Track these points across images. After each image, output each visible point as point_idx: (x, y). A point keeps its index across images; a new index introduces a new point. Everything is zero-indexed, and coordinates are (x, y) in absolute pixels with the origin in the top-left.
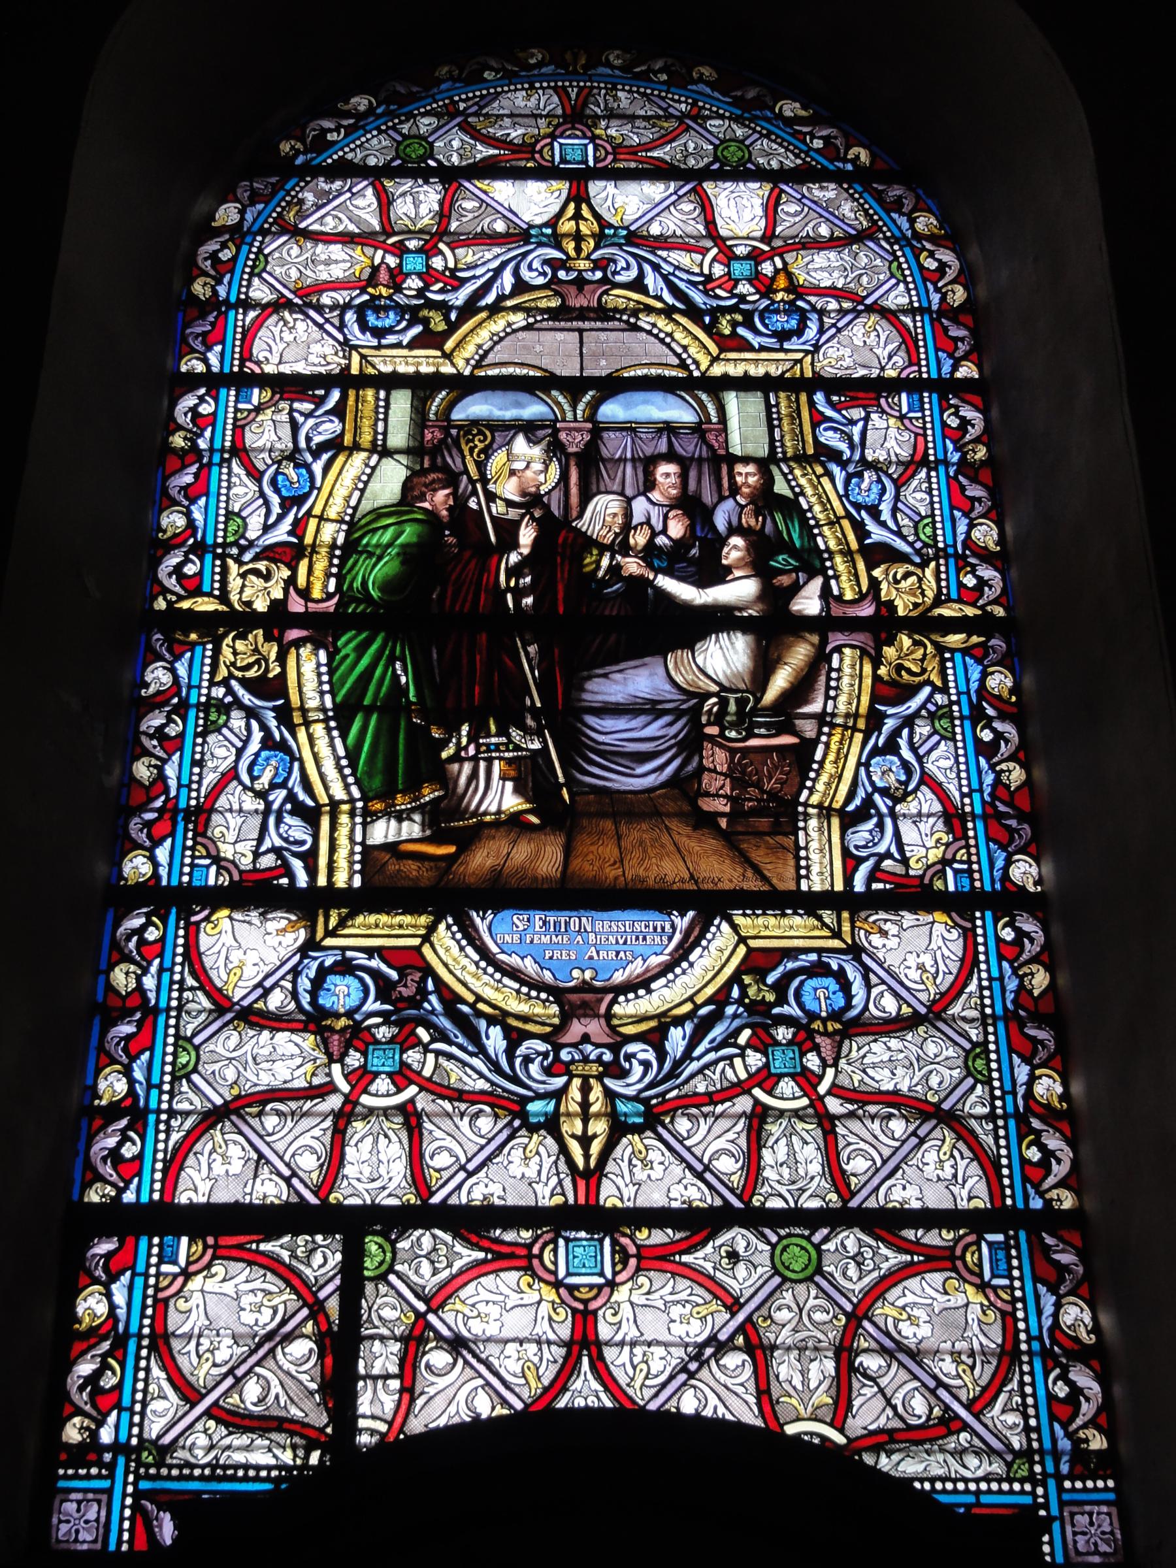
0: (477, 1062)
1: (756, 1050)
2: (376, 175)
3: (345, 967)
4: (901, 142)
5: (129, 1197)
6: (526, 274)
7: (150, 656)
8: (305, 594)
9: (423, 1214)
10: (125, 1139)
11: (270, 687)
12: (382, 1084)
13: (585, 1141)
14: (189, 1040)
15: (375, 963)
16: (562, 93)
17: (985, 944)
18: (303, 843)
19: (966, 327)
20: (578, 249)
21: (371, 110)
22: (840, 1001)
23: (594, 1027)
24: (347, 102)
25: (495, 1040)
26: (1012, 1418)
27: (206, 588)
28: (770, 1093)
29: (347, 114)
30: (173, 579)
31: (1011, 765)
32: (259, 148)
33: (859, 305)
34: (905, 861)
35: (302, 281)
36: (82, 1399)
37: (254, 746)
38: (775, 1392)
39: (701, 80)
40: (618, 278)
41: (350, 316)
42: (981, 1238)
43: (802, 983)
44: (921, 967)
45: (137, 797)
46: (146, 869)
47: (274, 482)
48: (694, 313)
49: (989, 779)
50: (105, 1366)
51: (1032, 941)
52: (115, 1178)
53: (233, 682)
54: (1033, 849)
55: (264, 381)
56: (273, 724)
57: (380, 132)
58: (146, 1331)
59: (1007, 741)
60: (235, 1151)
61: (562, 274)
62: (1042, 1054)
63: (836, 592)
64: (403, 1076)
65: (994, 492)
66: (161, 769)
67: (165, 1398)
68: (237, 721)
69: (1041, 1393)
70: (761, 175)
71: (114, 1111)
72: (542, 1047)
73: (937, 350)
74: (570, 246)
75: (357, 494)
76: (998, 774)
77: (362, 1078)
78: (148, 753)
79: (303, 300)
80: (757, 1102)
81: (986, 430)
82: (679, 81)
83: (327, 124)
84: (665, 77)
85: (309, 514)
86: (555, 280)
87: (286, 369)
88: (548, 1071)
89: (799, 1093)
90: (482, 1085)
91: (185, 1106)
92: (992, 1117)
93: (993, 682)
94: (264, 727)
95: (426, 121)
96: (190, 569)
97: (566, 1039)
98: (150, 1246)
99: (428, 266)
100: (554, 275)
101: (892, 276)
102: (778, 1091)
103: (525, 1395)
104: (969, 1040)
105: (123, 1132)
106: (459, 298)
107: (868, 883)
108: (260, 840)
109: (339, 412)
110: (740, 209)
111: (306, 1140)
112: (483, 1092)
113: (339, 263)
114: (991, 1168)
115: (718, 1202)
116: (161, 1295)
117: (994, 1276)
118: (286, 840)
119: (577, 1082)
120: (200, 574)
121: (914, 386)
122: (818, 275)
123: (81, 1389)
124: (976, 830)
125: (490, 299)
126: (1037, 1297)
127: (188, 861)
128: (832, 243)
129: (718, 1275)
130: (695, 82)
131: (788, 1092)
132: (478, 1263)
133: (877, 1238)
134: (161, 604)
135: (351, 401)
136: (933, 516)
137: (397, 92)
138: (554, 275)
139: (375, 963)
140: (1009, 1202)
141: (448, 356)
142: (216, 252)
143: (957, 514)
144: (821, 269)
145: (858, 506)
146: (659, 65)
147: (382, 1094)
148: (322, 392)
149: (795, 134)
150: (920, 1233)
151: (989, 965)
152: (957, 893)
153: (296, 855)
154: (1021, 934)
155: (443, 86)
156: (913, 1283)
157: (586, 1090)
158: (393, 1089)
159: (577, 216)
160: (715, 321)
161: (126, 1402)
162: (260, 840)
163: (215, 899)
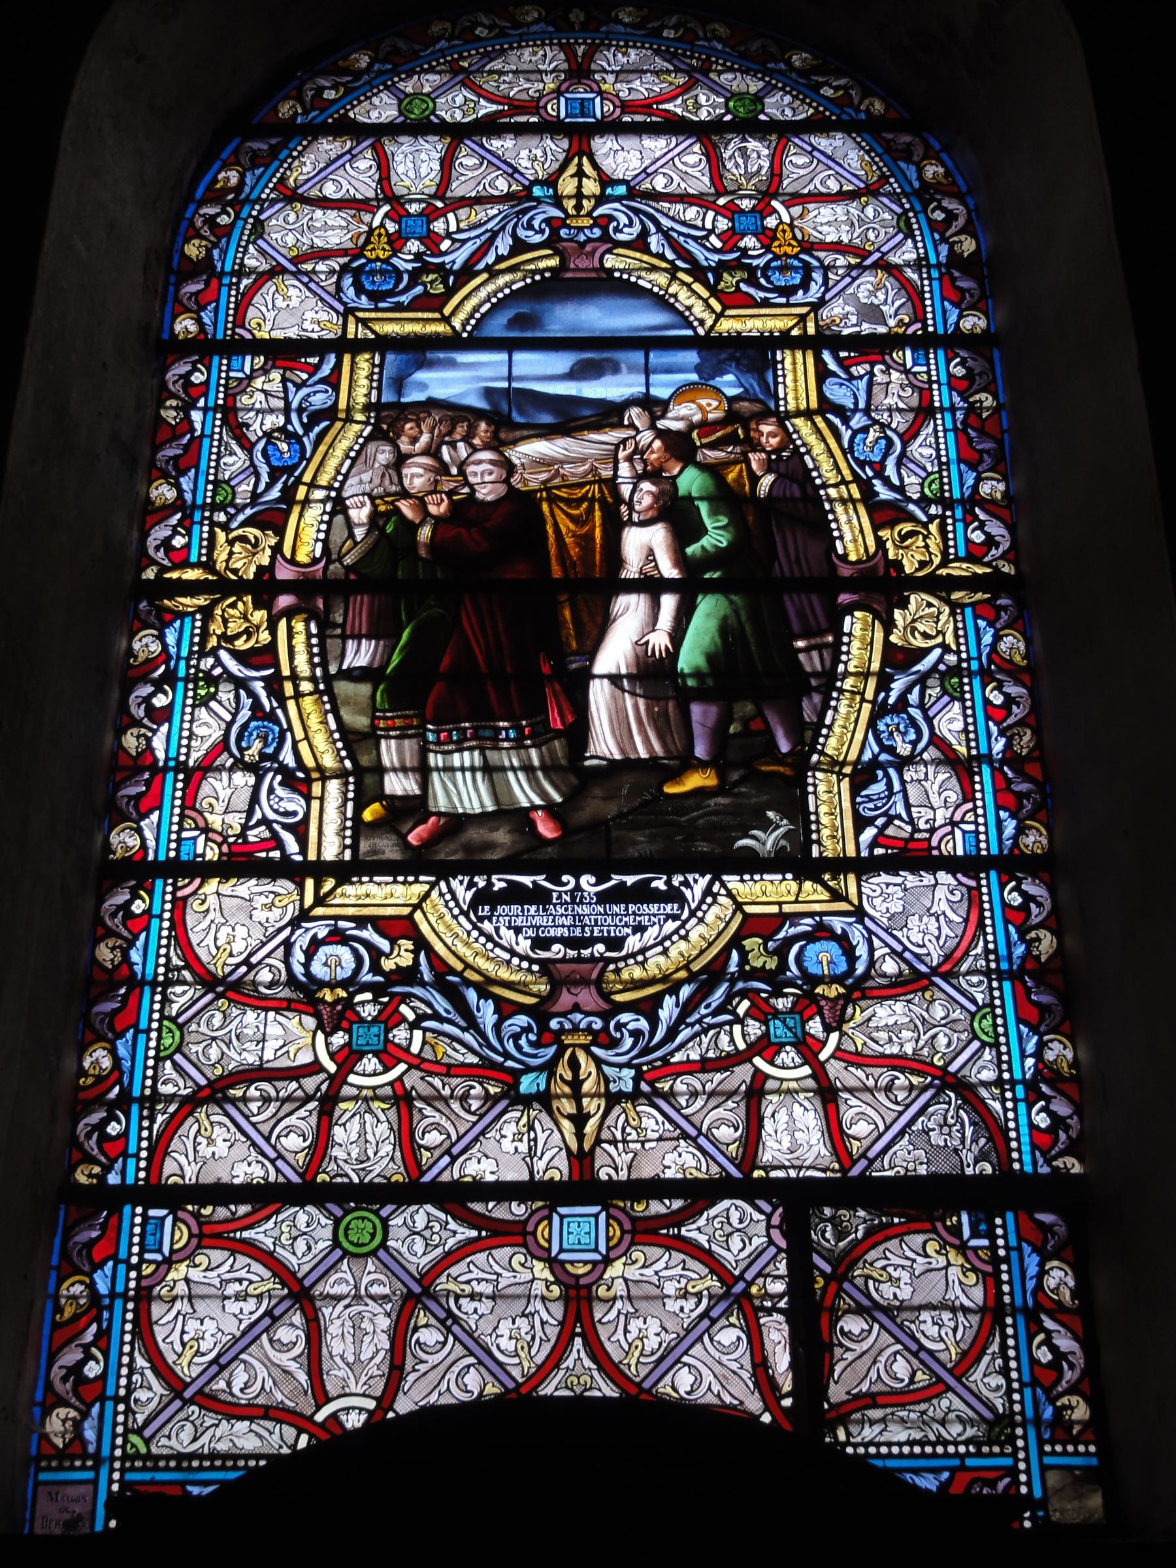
0: (468, 1037)
2: (708, 134)
3: (338, 937)
4: (911, 111)
5: (113, 1179)
7: (178, 308)
8: (292, 561)
9: (411, 1191)
10: (175, 532)
11: (263, 656)
12: (370, 1063)
14: (173, 1020)
15: (369, 934)
17: (991, 910)
18: (295, 813)
19: (1024, 686)
20: (579, 207)
22: (843, 967)
23: (587, 997)
25: (487, 1014)
27: (193, 558)
28: (771, 1063)
29: (345, 71)
30: (161, 554)
32: (254, 117)
33: (864, 260)
35: (296, 248)
36: (177, 388)
37: (245, 714)
40: (620, 237)
41: (348, 281)
43: (802, 949)
45: (163, 434)
46: (193, 328)
47: (264, 453)
48: (698, 271)
51: (1039, 905)
52: (125, 933)
55: (257, 346)
56: (263, 695)
58: (167, 915)
60: (219, 1133)
62: (1028, 805)
63: (840, 551)
64: (389, 1055)
65: (1020, 603)
66: (149, 740)
67: (150, 1389)
68: (226, 693)
69: (1023, 1120)
71: (168, 509)
73: (943, 299)
74: (570, 205)
75: (348, 462)
76: (951, 246)
77: (348, 1059)
78: (111, 933)
79: (298, 264)
81: (1034, 709)
87: (278, 334)
89: (798, 1060)
90: (472, 1059)
91: (168, 1089)
92: (999, 1082)
93: (985, 489)
94: (251, 694)
96: (113, 1129)
97: (557, 1008)
98: (134, 1215)
102: (778, 1061)
103: (516, 1373)
104: (974, 1001)
106: (460, 257)
108: (250, 813)
110: (750, 158)
113: (334, 230)
114: (994, 1131)
116: (180, 894)
118: (276, 811)
120: (188, 546)
121: (923, 343)
123: (157, 548)
125: (490, 258)
126: (944, 311)
128: (841, 196)
129: (714, 1248)
131: (788, 1062)
132: (470, 1241)
134: (150, 574)
139: (369, 934)
141: (447, 320)
143: (1003, 814)
145: (862, 464)
147: (369, 1074)
148: (315, 360)
151: (996, 932)
152: (966, 856)
153: (286, 827)
154: (1027, 898)
156: (480, 1258)
158: (380, 1068)
159: (580, 174)
160: (718, 279)
161: (132, 1149)
162: (250, 813)
163: (203, 870)
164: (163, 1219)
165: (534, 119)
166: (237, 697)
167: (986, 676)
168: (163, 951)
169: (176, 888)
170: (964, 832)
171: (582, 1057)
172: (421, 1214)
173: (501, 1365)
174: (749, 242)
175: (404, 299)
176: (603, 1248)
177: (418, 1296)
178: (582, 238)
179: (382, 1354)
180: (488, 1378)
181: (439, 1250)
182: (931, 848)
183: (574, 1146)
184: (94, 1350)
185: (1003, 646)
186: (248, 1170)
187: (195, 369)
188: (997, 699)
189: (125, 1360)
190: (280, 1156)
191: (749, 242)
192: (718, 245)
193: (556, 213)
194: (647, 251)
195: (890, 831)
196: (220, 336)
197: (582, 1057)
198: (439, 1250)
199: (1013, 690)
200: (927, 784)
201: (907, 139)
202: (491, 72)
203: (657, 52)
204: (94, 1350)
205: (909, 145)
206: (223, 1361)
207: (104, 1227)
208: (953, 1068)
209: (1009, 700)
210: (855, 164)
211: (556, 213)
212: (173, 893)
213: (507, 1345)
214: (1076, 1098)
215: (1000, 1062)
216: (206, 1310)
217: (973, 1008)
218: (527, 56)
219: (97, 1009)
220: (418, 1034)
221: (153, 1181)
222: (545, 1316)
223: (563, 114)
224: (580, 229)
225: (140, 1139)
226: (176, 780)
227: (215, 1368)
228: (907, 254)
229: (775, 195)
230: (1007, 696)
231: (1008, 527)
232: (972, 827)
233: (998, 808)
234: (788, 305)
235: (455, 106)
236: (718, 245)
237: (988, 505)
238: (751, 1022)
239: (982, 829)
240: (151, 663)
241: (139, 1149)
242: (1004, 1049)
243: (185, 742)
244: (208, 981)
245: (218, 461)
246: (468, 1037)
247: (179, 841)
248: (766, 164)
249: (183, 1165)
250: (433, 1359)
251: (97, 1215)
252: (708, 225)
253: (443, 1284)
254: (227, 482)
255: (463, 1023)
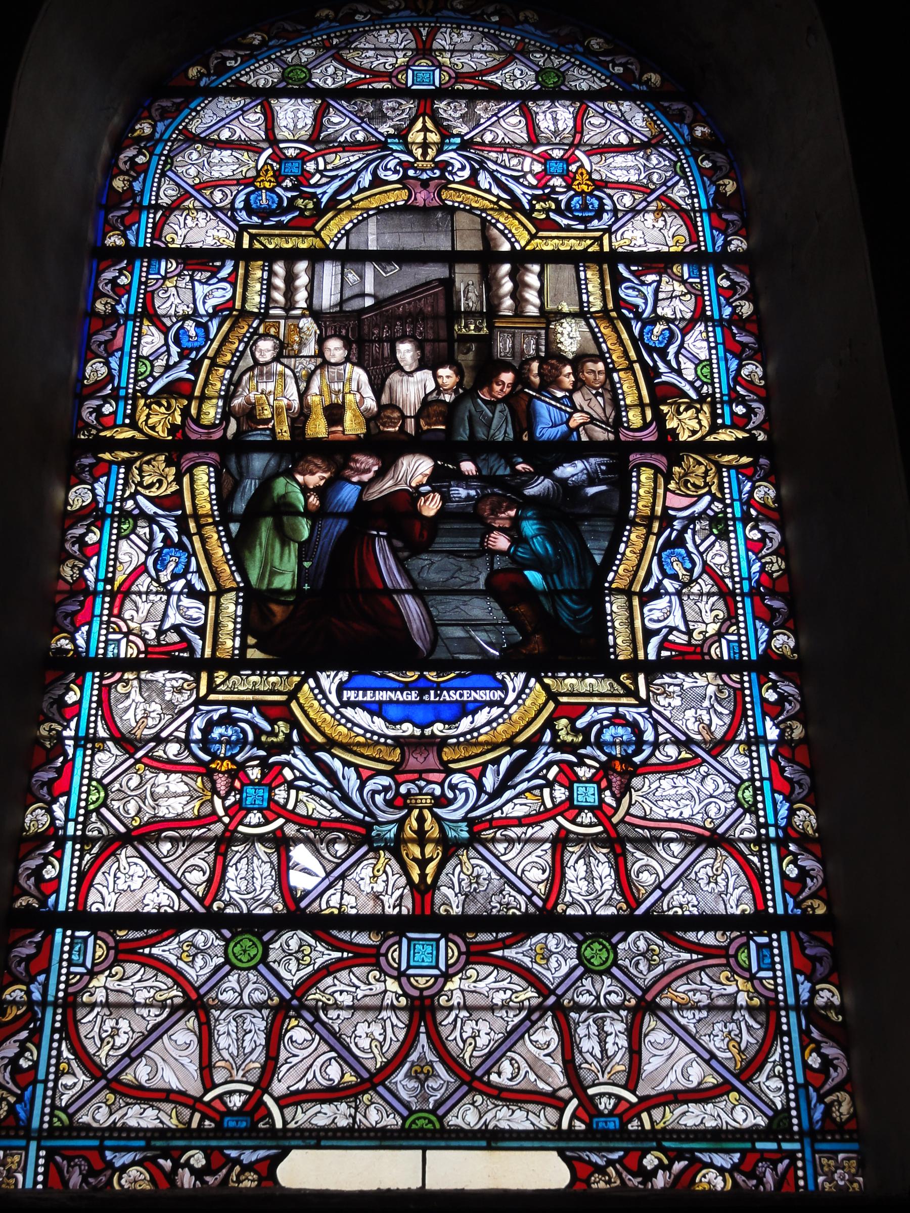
1: (561, 785)
2: (523, 98)
6: (381, 174)
7: (107, 228)
12: (254, 817)
13: (423, 863)
16: (416, 32)
19: (825, 945)
20: (424, 154)
21: (263, 43)
24: (244, 36)
26: (776, 1083)
31: (774, 558)
34: (689, 633)
38: (578, 1059)
39: (526, 20)
42: (750, 938)
44: (699, 720)
49: (756, 567)
50: (23, 1049)
53: (139, 498)
54: (790, 624)
57: (270, 60)
59: (771, 540)
61: (411, 173)
70: (575, 96)
71: (41, 839)
72: (386, 781)
74: (418, 152)
77: (238, 810)
80: (561, 827)
82: (508, 23)
83: (228, 53)
84: (495, 19)
85: (205, 356)
86: (405, 176)
88: (388, 803)
92: (758, 841)
95: (307, 51)
99: (303, 170)
100: (405, 173)
101: (676, 174)
103: (370, 1065)
105: (89, 526)
107: (659, 653)
109: (231, 280)
110: (556, 118)
111: (195, 861)
112: (336, 820)
114: (756, 879)
115: (185, 907)
116: (105, 682)
117: (760, 969)
119: (416, 812)
122: (618, 172)
124: (745, 608)
126: (713, 237)
127: (103, 638)
130: (522, 23)
133: (663, 938)
135: (241, 271)
136: (710, 360)
137: (285, 30)
138: (405, 173)
140: (771, 910)
141: (318, 235)
142: (100, 407)
144: (623, 169)
146: (491, 9)
149: (600, 63)
150: (701, 933)
155: (322, 26)
156: (343, 975)
157: (421, 819)
161: (41, 1076)
164: (85, 940)
165: (387, 86)
166: (152, 533)
167: (746, 519)
168: (55, 1045)
169: (102, 678)
170: (729, 642)
171: (427, 813)
172: (293, 939)
173: (356, 1058)
174: (557, 182)
175: (285, 219)
176: (442, 966)
177: (286, 1008)
178: (425, 176)
179: (260, 1049)
180: (346, 1068)
181: (310, 968)
182: (703, 654)
183: (416, 879)
184: (29, 1045)
185: (744, 372)
186: (159, 899)
187: (89, 531)
188: (814, 1061)
189: (54, 1053)
190: (184, 887)
191: (557, 182)
192: (534, 182)
193: (405, 157)
194: (478, 187)
195: (671, 637)
196: (141, 245)
197: (427, 813)
198: (310, 968)
199: (808, 863)
200: (665, 232)
201: (680, 106)
202: (356, 49)
203: (485, 35)
204: (29, 1045)
205: (681, 110)
206: (134, 1054)
207: (39, 945)
208: (720, 830)
209: (804, 872)
210: (640, 123)
211: (405, 157)
212: (65, 990)
213: (365, 1043)
214: (819, 854)
215: (730, 551)
216: (121, 1005)
217: (737, 781)
218: (386, 37)
219: (95, 338)
220: (293, 792)
221: (80, 908)
222: (395, 1021)
223: (410, 83)
224: (424, 170)
225: (79, 808)
226: (103, 602)
227: (127, 1061)
228: (746, 828)
229: (577, 146)
230: (801, 869)
231: (818, 860)
232: (735, 638)
233: (795, 971)
234: (586, 230)
235: (328, 75)
236: (534, 182)
237: (803, 840)
238: (557, 787)
239: (743, 638)
240: (100, 385)
241: (78, 815)
242: (761, 813)
243: (84, 796)
244: (127, 743)
245: (56, 1081)
246: (494, 167)
247: (107, 642)
248: (571, 124)
249: (105, 897)
250: (303, 1054)
251: (32, 935)
252: (526, 169)
253: (314, 996)
254: (147, 358)
255: (329, 786)
